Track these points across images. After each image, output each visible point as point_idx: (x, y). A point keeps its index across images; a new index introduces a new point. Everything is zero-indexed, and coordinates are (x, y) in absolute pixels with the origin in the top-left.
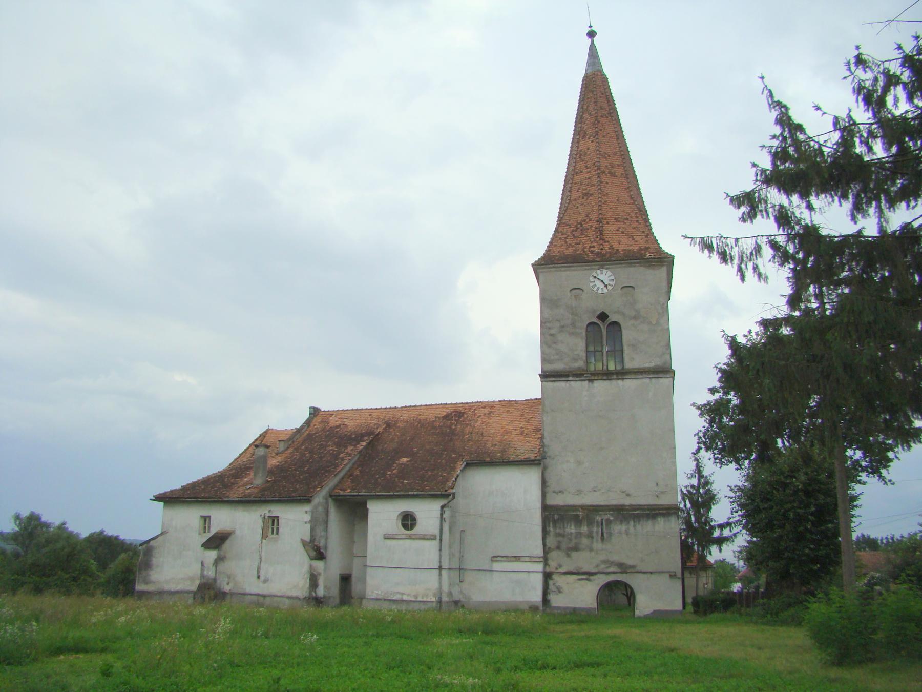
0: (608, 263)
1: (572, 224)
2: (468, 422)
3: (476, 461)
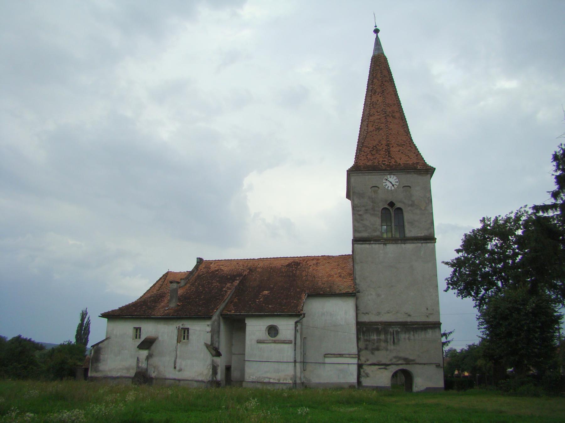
1: (370, 146)
2: (303, 269)
3: (314, 294)
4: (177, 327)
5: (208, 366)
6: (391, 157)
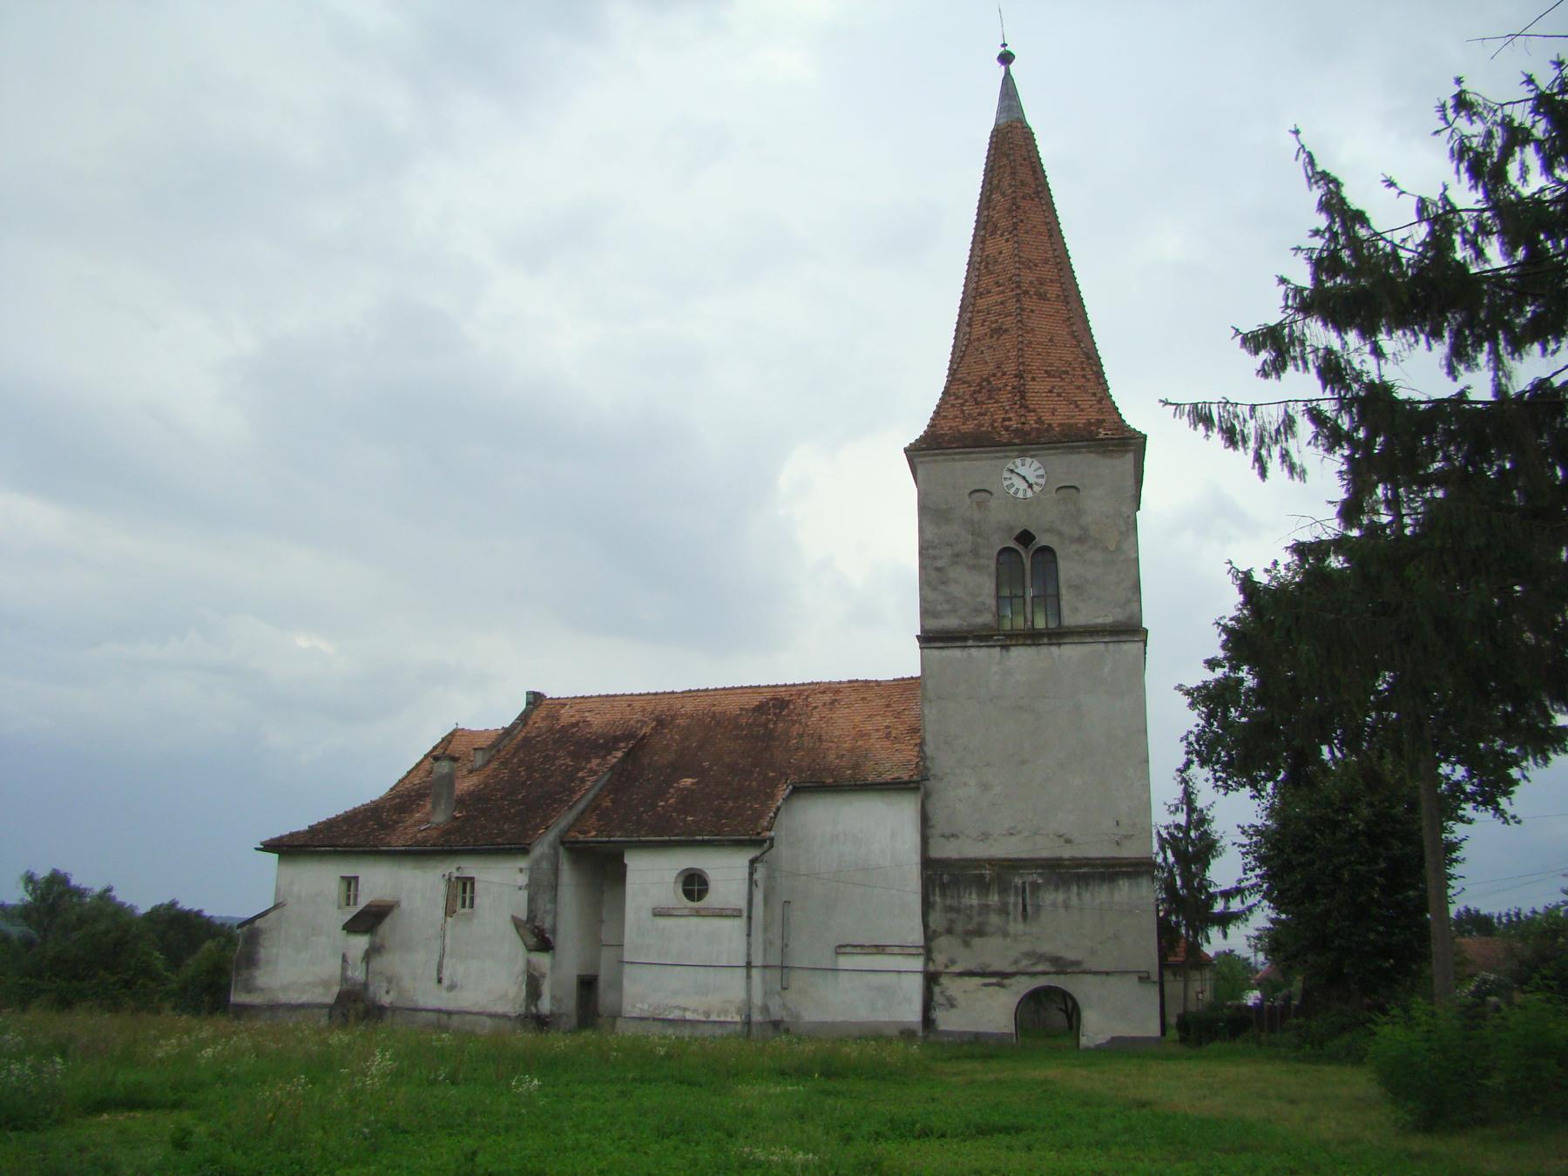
0: (1034, 446)
2: (795, 718)
3: (809, 784)
4: (444, 875)
5: (518, 977)
6: (1027, 407)
